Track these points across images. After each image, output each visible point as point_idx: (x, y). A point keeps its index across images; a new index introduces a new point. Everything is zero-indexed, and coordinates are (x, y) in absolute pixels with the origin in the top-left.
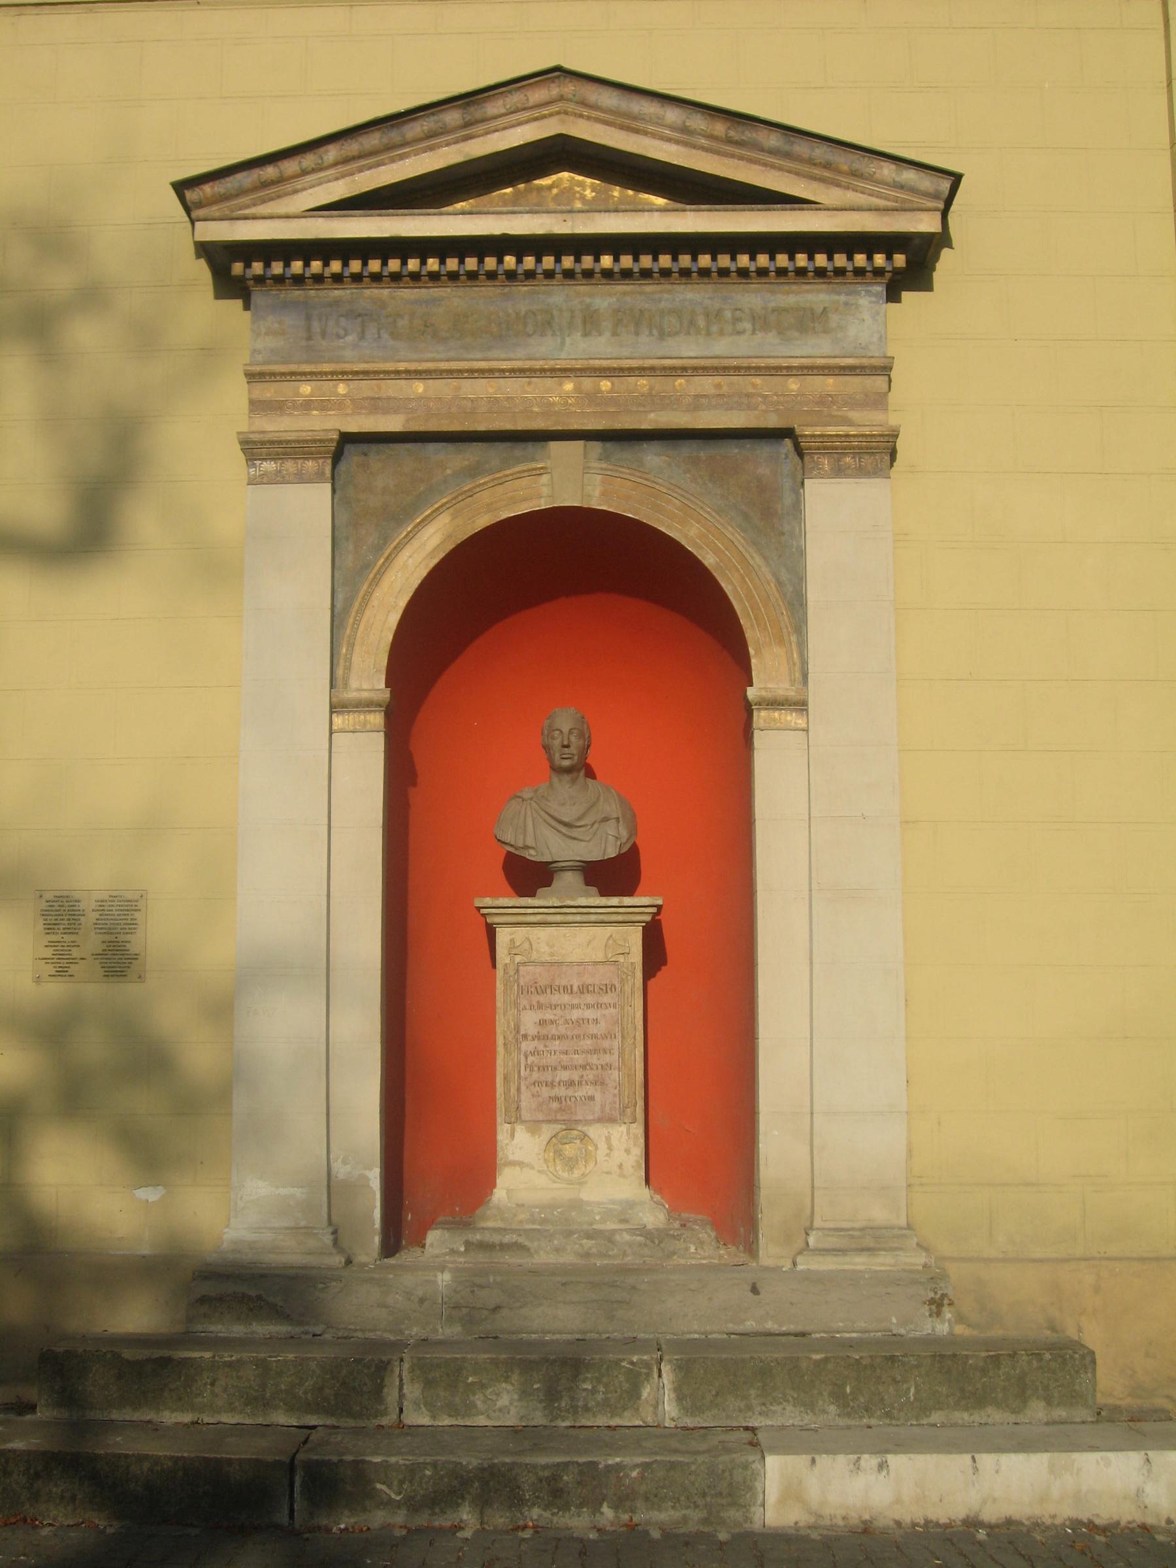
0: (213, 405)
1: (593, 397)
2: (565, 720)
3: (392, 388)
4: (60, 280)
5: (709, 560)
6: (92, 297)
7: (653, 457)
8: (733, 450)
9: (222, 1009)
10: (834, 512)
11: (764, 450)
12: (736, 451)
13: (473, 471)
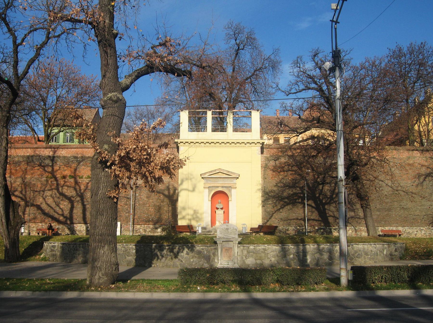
0: (201, 184)
2: (219, 201)
4: (192, 177)
6: (193, 178)
9: (201, 214)
10: (233, 191)
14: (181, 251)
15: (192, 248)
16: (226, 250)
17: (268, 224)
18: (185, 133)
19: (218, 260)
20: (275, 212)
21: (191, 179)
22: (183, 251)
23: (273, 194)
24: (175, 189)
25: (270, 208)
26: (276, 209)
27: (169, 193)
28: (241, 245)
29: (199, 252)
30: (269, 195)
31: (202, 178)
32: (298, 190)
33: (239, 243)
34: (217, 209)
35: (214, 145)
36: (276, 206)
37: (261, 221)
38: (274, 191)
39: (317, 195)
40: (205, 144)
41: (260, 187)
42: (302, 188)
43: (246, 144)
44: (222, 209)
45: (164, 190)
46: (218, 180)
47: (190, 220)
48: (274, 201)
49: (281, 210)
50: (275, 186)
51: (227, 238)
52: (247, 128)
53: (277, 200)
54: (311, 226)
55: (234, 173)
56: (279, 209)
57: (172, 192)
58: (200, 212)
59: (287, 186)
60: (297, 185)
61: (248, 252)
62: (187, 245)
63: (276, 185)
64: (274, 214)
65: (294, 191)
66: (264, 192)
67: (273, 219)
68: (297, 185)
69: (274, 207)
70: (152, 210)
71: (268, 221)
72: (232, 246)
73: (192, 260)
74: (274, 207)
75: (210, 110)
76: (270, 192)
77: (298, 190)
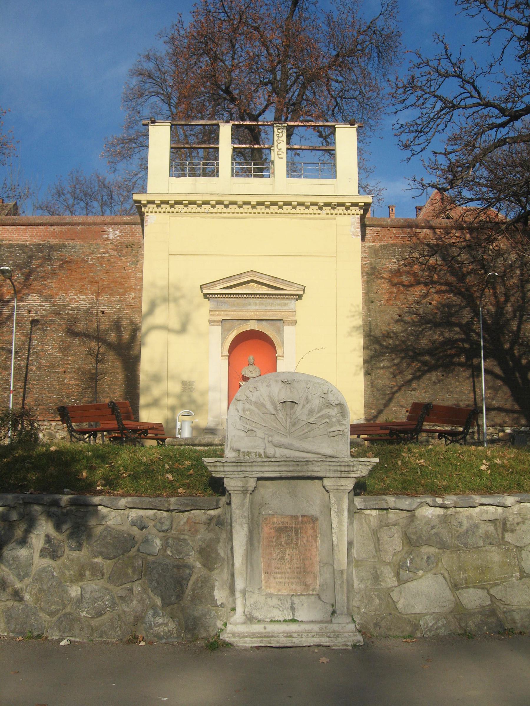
0: (203, 313)
1: (256, 315)
2: (251, 357)
3: (229, 313)
4: (178, 294)
5: (271, 337)
6: (183, 297)
7: (264, 323)
8: (275, 322)
9: (204, 393)
10: (287, 330)
11: (279, 322)
12: (41, 435)
13: (240, 324)
14: (19, 533)
15: (77, 522)
16: (282, 530)
17: (382, 419)
18: (160, 177)
20: (399, 389)
21: (176, 300)
22: (28, 531)
23: (391, 341)
24: (135, 329)
25: (384, 378)
26: (400, 379)
27: (120, 336)
28: (374, 501)
29: (122, 546)
30: (380, 344)
31: (206, 296)
32: (457, 333)
33: (360, 488)
35: (238, 210)
36: (401, 372)
37: (363, 412)
38: (395, 333)
39: (507, 346)
40: (213, 207)
41: (359, 322)
42: (467, 328)
43: (321, 208)
45: (106, 331)
46: (247, 301)
47: (173, 409)
48: (397, 361)
49: (414, 385)
50: (397, 321)
51: (286, 461)
53: (403, 358)
54: (493, 426)
55: (290, 284)
56: (410, 381)
57: (126, 335)
58: (199, 386)
59: (429, 322)
60: (453, 319)
61: (412, 542)
62: (47, 498)
63: (400, 320)
64: (397, 395)
65: (447, 335)
66: (370, 336)
67: (393, 407)
68: (453, 319)
69: (395, 376)
70: (73, 382)
71: (380, 412)
72: (314, 510)
73: (74, 591)
74: (395, 376)
75: (227, 122)
76: (384, 336)
77: (456, 333)
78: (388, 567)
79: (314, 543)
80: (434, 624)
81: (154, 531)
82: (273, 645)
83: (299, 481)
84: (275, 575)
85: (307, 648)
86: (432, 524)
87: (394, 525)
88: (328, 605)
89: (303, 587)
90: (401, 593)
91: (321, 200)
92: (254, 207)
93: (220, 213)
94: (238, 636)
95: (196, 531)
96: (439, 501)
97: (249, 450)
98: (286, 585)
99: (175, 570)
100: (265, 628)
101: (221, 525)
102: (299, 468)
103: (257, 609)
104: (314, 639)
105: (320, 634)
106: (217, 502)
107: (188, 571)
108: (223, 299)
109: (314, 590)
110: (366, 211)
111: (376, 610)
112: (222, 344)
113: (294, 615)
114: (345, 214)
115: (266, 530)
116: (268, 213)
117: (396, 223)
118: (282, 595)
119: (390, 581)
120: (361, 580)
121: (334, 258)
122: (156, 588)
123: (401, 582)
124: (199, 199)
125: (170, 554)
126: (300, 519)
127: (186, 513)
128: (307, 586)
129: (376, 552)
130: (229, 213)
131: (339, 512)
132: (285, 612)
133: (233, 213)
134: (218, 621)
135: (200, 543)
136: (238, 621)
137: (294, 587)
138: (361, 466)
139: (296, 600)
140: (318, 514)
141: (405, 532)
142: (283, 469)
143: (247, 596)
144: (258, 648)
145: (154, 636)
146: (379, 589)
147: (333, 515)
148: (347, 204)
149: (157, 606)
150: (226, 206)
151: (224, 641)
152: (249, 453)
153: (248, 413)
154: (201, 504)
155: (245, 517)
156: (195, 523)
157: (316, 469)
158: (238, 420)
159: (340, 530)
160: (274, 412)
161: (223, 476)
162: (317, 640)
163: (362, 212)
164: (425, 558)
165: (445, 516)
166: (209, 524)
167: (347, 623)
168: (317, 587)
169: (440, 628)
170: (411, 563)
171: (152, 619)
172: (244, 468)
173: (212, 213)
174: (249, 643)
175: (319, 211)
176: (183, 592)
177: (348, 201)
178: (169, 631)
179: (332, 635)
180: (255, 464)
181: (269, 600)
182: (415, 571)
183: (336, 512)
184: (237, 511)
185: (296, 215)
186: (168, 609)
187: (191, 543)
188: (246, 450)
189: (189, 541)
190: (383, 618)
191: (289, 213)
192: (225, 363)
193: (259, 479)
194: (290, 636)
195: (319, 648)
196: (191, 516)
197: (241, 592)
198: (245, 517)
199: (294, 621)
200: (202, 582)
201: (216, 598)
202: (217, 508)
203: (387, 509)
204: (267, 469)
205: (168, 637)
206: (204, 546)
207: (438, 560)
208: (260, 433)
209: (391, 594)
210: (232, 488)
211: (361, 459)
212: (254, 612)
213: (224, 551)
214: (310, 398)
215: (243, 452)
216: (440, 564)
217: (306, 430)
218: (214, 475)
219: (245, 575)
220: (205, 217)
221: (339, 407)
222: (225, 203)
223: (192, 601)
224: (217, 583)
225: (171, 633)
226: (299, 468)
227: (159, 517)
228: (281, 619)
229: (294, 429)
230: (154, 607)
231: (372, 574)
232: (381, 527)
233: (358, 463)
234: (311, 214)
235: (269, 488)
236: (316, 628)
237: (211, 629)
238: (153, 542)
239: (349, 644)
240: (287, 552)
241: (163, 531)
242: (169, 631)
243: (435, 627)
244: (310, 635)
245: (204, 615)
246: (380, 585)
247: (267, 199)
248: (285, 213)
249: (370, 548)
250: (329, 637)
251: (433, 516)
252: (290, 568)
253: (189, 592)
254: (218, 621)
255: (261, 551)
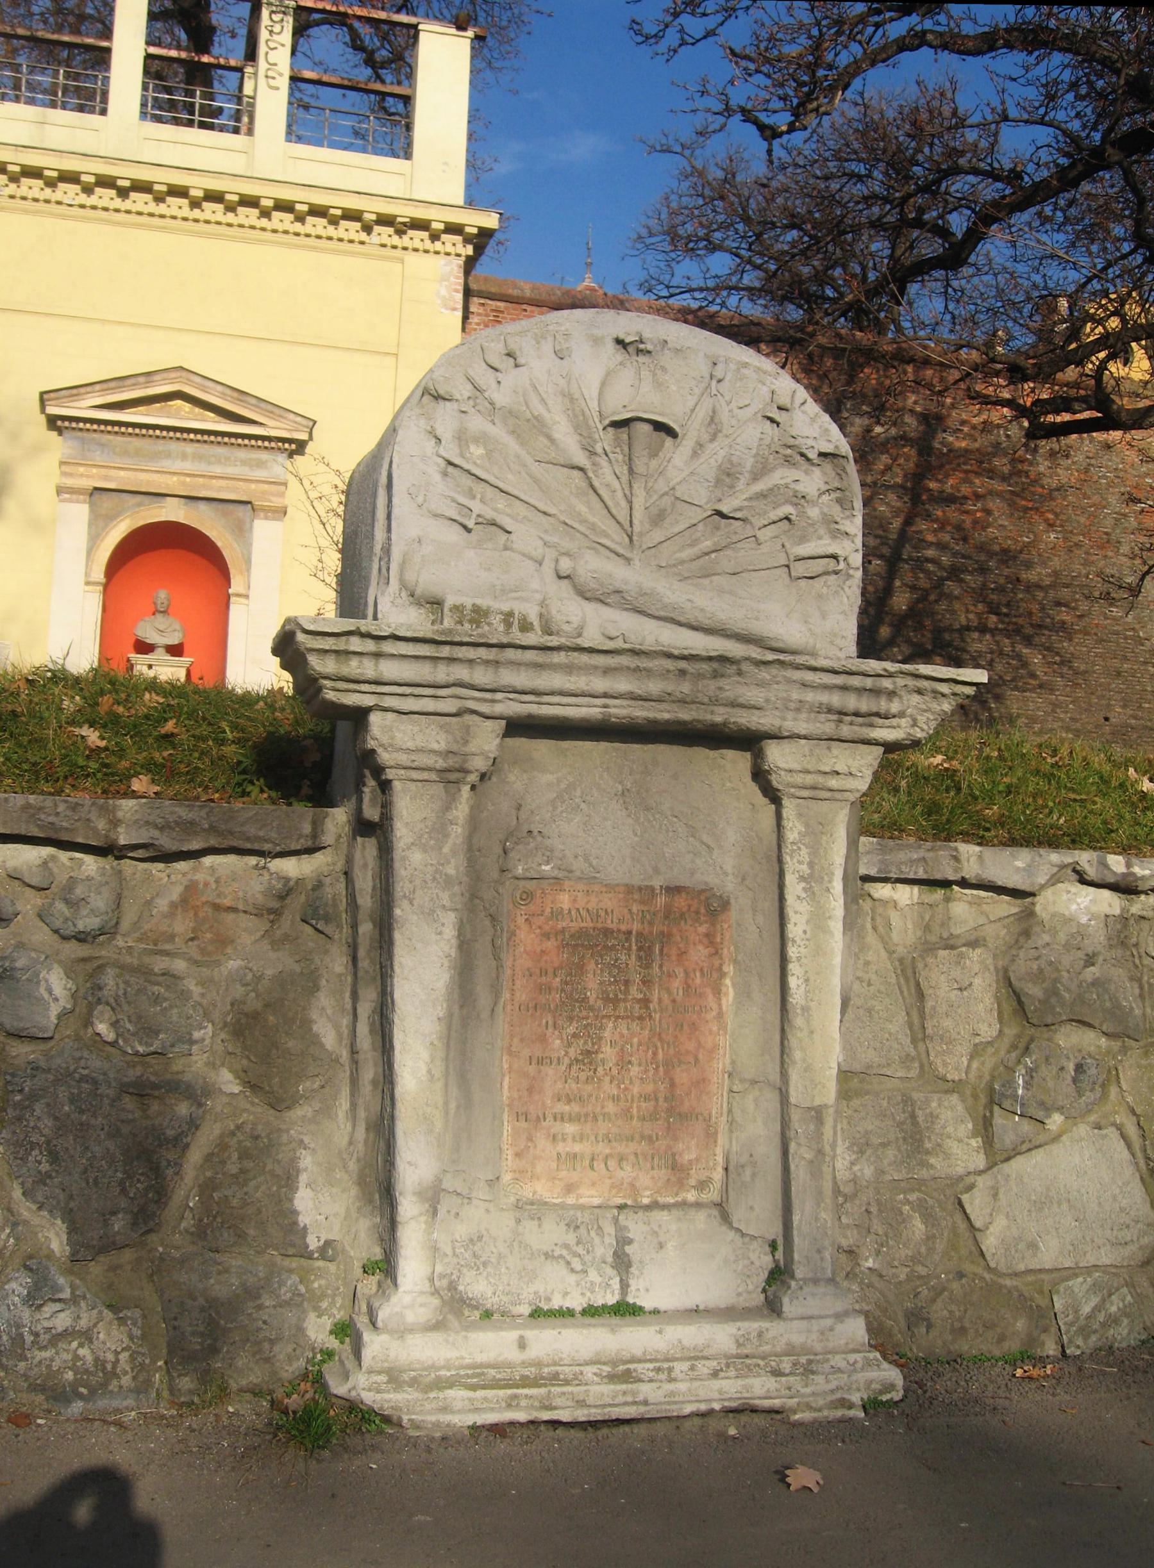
1: (184, 483)
2: (162, 595)
3: (113, 473)
5: (219, 544)
7: (203, 506)
8: (231, 507)
10: (263, 530)
11: (241, 507)
13: (140, 505)
16: (589, 942)
19: (381, 1190)
34: (144, 648)
35: (152, 207)
40: (88, 190)
43: (368, 229)
44: (175, 650)
46: (161, 446)
52: (387, 119)
55: (277, 410)
61: (1028, 1009)
78: (954, 1099)
79: (711, 1000)
80: (1097, 1309)
81: (41, 935)
82: (564, 1416)
83: (661, 748)
84: (557, 1127)
85: (697, 1421)
86: (1090, 946)
87: (974, 944)
88: (755, 1245)
89: (663, 1174)
90: (995, 1196)
91: (371, 208)
92: (195, 204)
93: (106, 209)
94: (414, 1382)
95: (223, 942)
96: (1117, 863)
97: (483, 603)
98: (599, 1165)
99: (129, 1102)
100: (522, 1345)
101: (327, 919)
102: (686, 688)
103: (480, 1264)
104: (716, 1384)
105: (740, 1361)
106: (317, 826)
107: (183, 1109)
108: (95, 435)
109: (702, 1185)
110: (479, 250)
111: (916, 1259)
112: (90, 552)
113: (624, 1286)
114: (427, 251)
115: (527, 938)
116: (230, 225)
117: (544, 296)
118: (582, 1208)
119: (962, 1152)
120: (861, 1147)
121: (391, 361)
122: (43, 1179)
123: (997, 1155)
124: (52, 163)
125: (110, 1036)
126: (661, 900)
127: (182, 866)
128: (678, 1170)
129: (914, 1041)
130: (128, 212)
131: (814, 879)
132: (593, 1275)
133: (140, 213)
134: (312, 1315)
135: (239, 991)
136: (410, 1317)
137: (626, 1173)
138: (916, 699)
139: (635, 1226)
140: (729, 886)
141: (1006, 970)
142: (623, 685)
143: (442, 1210)
144: (498, 1430)
145: (34, 1388)
146: (922, 1182)
147: (794, 888)
148: (435, 225)
149: (50, 1256)
150: (123, 193)
151: (352, 1406)
152: (479, 615)
153: (477, 451)
154: (252, 830)
155: (448, 882)
156: (217, 907)
157: (753, 695)
158: (437, 477)
159: (819, 951)
160: (581, 459)
161: (367, 701)
162: (728, 1389)
163: (469, 250)
164: (1071, 1067)
165: (1124, 919)
166: (277, 913)
167: (840, 1316)
168: (718, 1175)
169: (1114, 1320)
170: (1028, 1085)
171: (26, 1314)
172: (461, 673)
173: (82, 206)
174: (464, 1410)
175: (363, 236)
176: (160, 1193)
177: (438, 217)
178: (99, 1362)
179: (786, 1366)
180: (510, 654)
181: (529, 1226)
182: (1040, 1115)
183: (802, 878)
184: (417, 857)
185: (303, 240)
186: (96, 1269)
187: (196, 990)
188: (468, 602)
189: (191, 985)
190: (938, 1291)
191: (286, 232)
192: (92, 605)
193: (517, 727)
194: (627, 1377)
195: (744, 1418)
196: (200, 877)
197: (420, 1194)
198: (448, 882)
199: (625, 1310)
200: (244, 1155)
201: (303, 1220)
202: (310, 851)
203: (945, 884)
204: (557, 681)
205: (93, 1392)
206: (253, 1004)
207: (1112, 1076)
208: (527, 536)
209: (965, 1198)
210: (403, 759)
211: (925, 669)
212: (468, 1276)
213: (337, 1027)
214: (724, 415)
215: (458, 609)
216: (1113, 1091)
217: (707, 544)
218: (330, 695)
219: (439, 1125)
220: (64, 217)
221: (828, 466)
222: (120, 183)
223: (201, 1233)
224: (306, 1161)
225: (106, 1373)
226: (686, 688)
227: (62, 878)
228: (576, 1302)
229: (657, 535)
230: (35, 1265)
231: (900, 1124)
232: (929, 949)
233: (911, 682)
234: (340, 240)
235: (552, 765)
236: (722, 1337)
237: (281, 1351)
238: (35, 980)
239: (856, 1398)
240: (607, 1034)
241: (81, 938)
242: (99, 1362)
243: (1101, 1317)
244: (704, 1368)
245: (251, 1293)
246: (924, 1164)
247: (233, 188)
248: (275, 231)
249: (892, 1028)
250: (777, 1373)
251: (1093, 917)
252: (615, 1099)
253: (185, 1191)
254: (312, 1315)
255: (502, 1024)
